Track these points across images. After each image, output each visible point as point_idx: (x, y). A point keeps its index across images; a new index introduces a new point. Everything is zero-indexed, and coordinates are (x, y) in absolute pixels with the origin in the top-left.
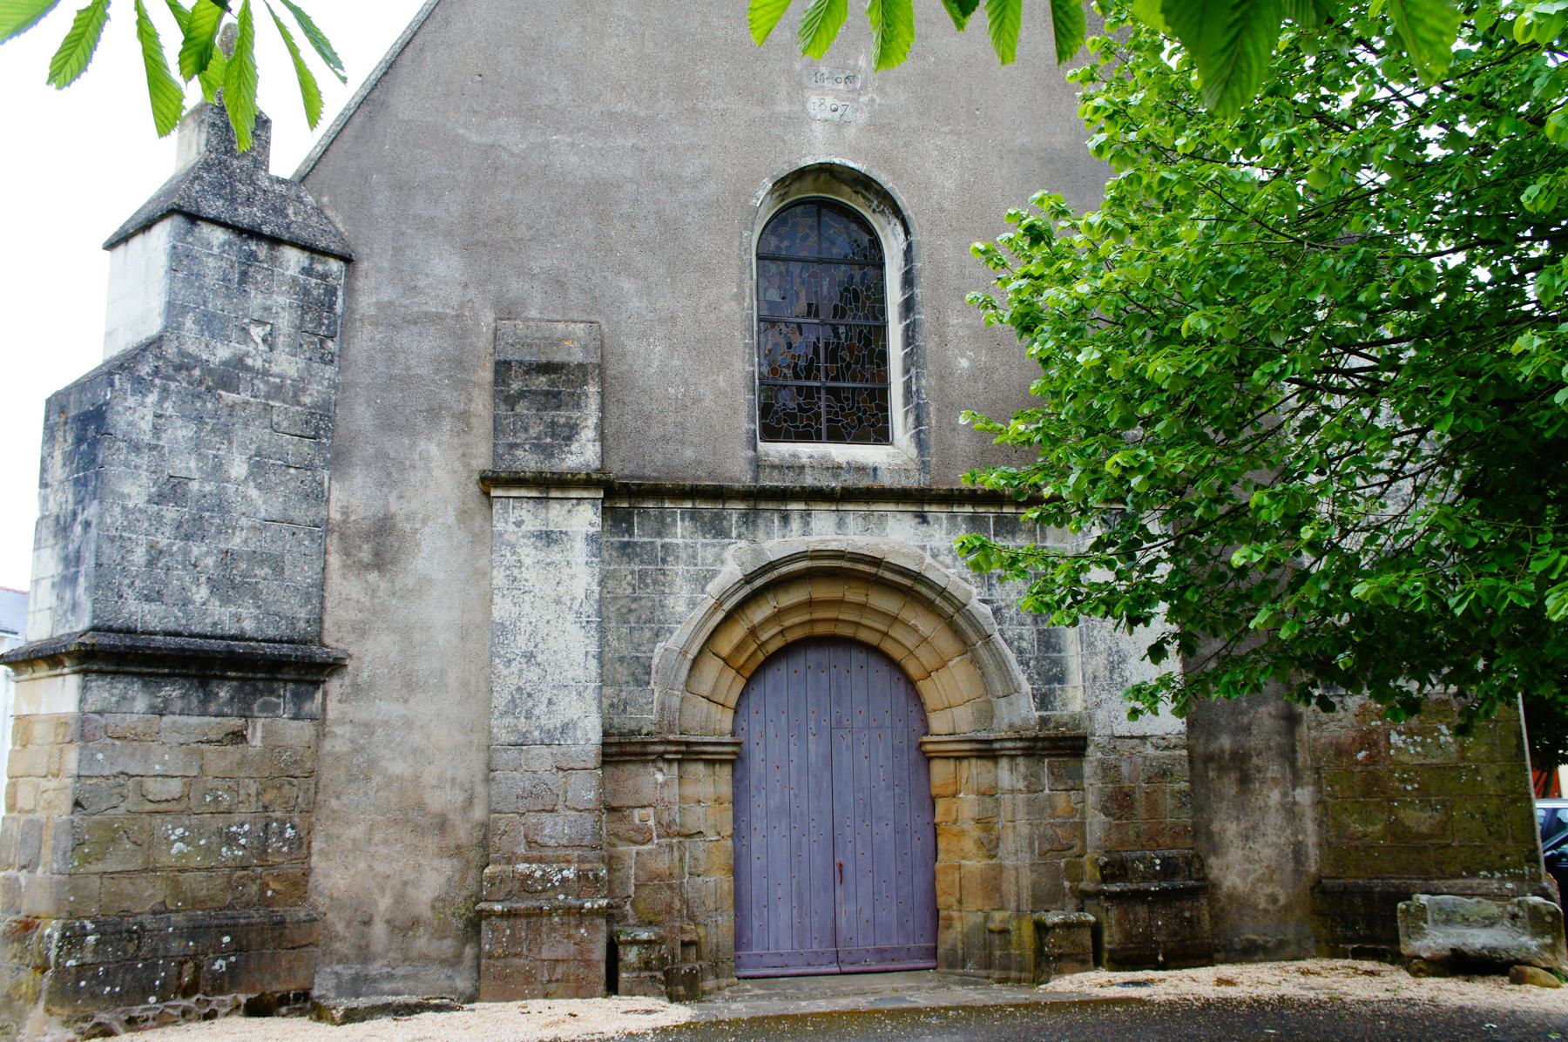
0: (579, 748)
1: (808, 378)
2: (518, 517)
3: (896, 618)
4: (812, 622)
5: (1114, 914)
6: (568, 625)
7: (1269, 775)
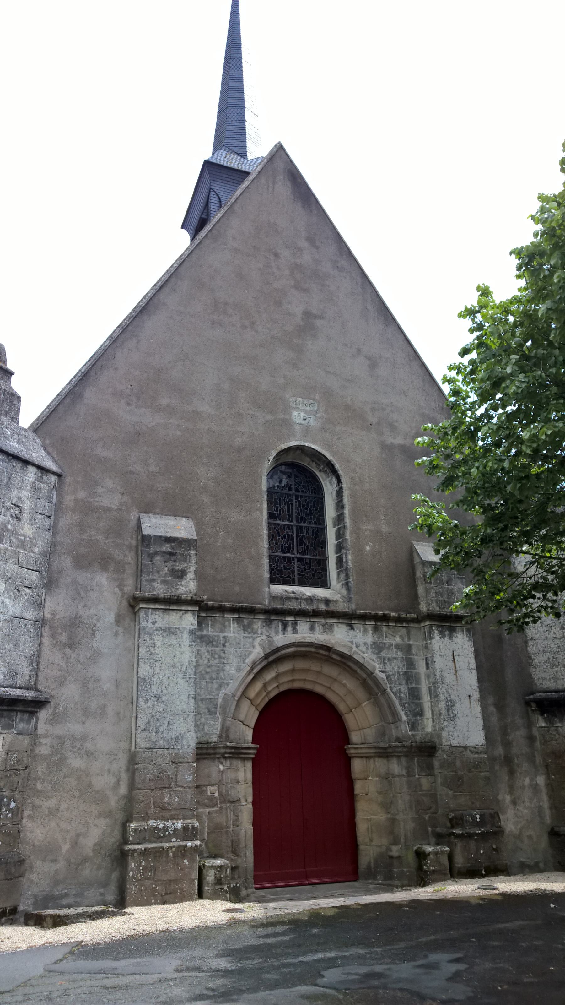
0: (185, 750)
1: (288, 552)
2: (154, 619)
3: (335, 680)
4: (293, 681)
5: (459, 846)
6: (179, 679)
7: (524, 769)
